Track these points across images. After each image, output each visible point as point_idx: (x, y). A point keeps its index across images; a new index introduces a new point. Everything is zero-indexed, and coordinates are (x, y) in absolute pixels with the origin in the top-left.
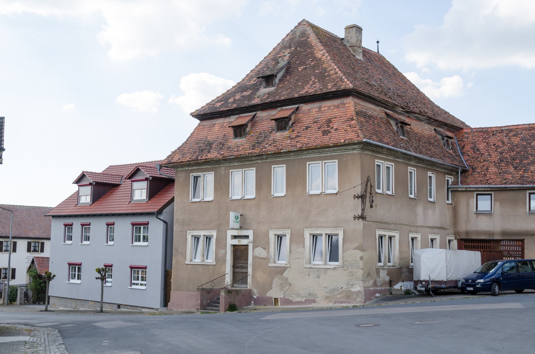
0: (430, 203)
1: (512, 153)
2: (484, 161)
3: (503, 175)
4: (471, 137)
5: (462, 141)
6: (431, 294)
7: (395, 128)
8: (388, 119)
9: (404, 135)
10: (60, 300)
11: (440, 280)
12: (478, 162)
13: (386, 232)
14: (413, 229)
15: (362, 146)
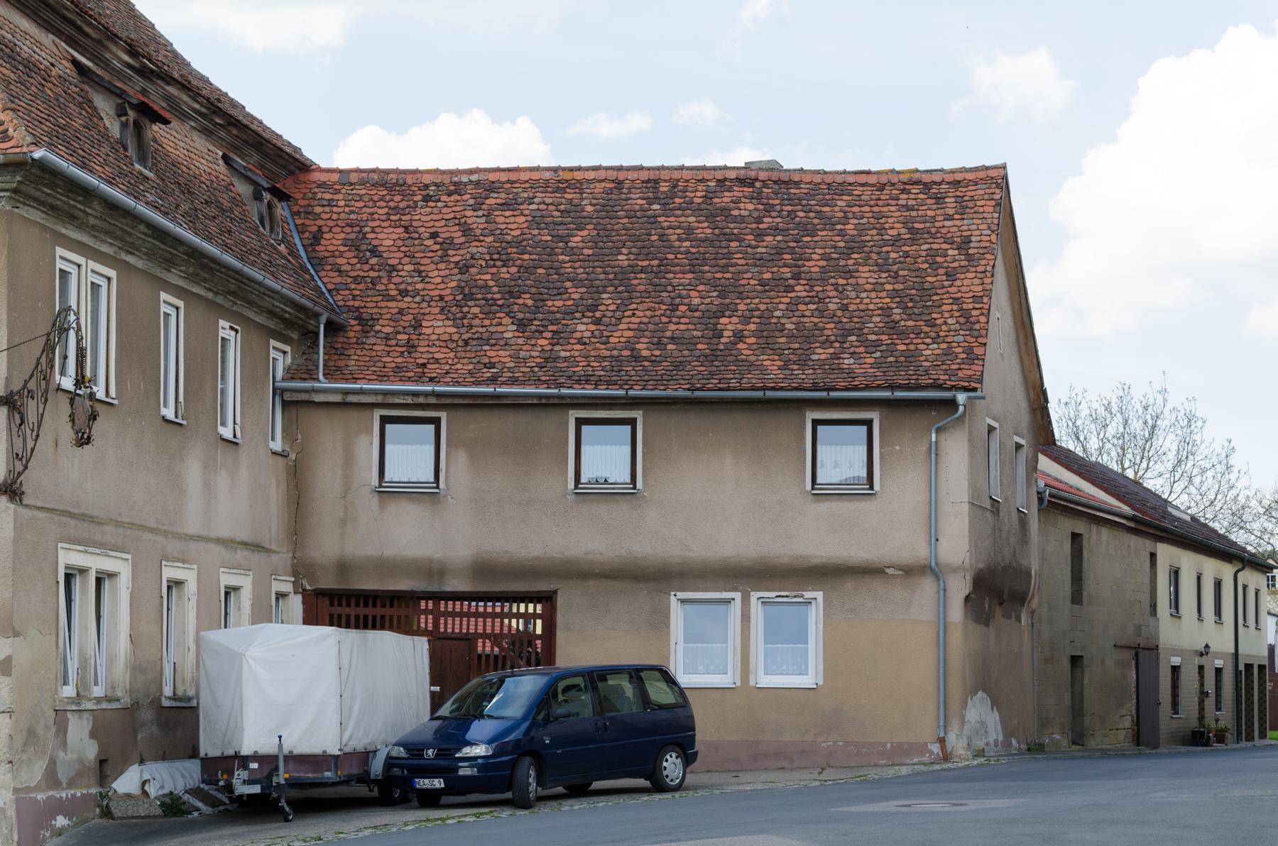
0: (225, 443)
1: (504, 270)
2: (404, 293)
3: (479, 348)
4: (342, 203)
5: (309, 213)
6: (285, 811)
7: (114, 127)
8: (86, 88)
9: (142, 160)
11: (317, 750)
12: (380, 298)
13: (89, 555)
14: (173, 546)
15: (19, 178)
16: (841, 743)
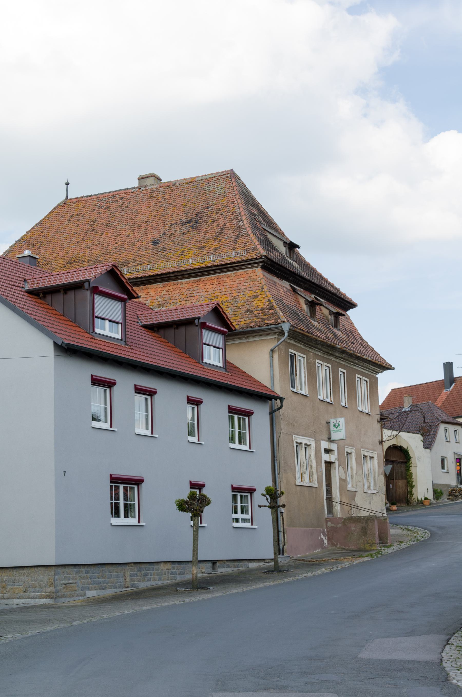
10: (87, 572)
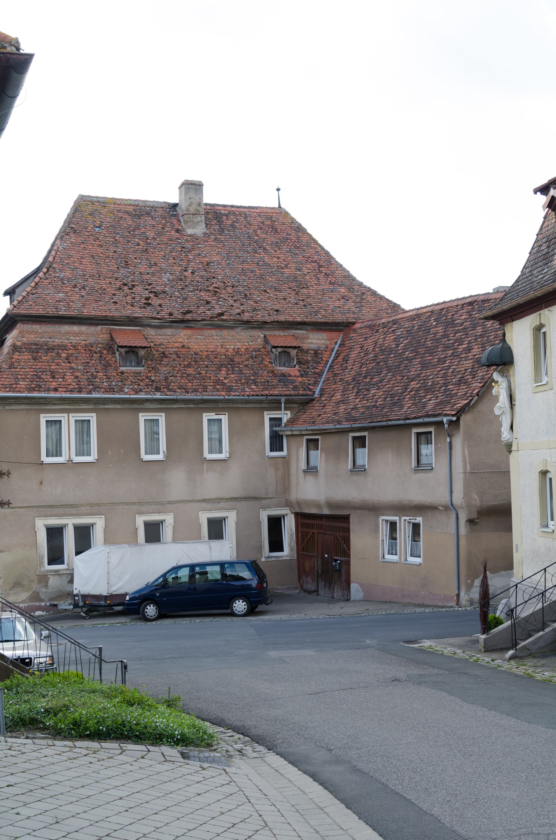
16: (427, 593)
